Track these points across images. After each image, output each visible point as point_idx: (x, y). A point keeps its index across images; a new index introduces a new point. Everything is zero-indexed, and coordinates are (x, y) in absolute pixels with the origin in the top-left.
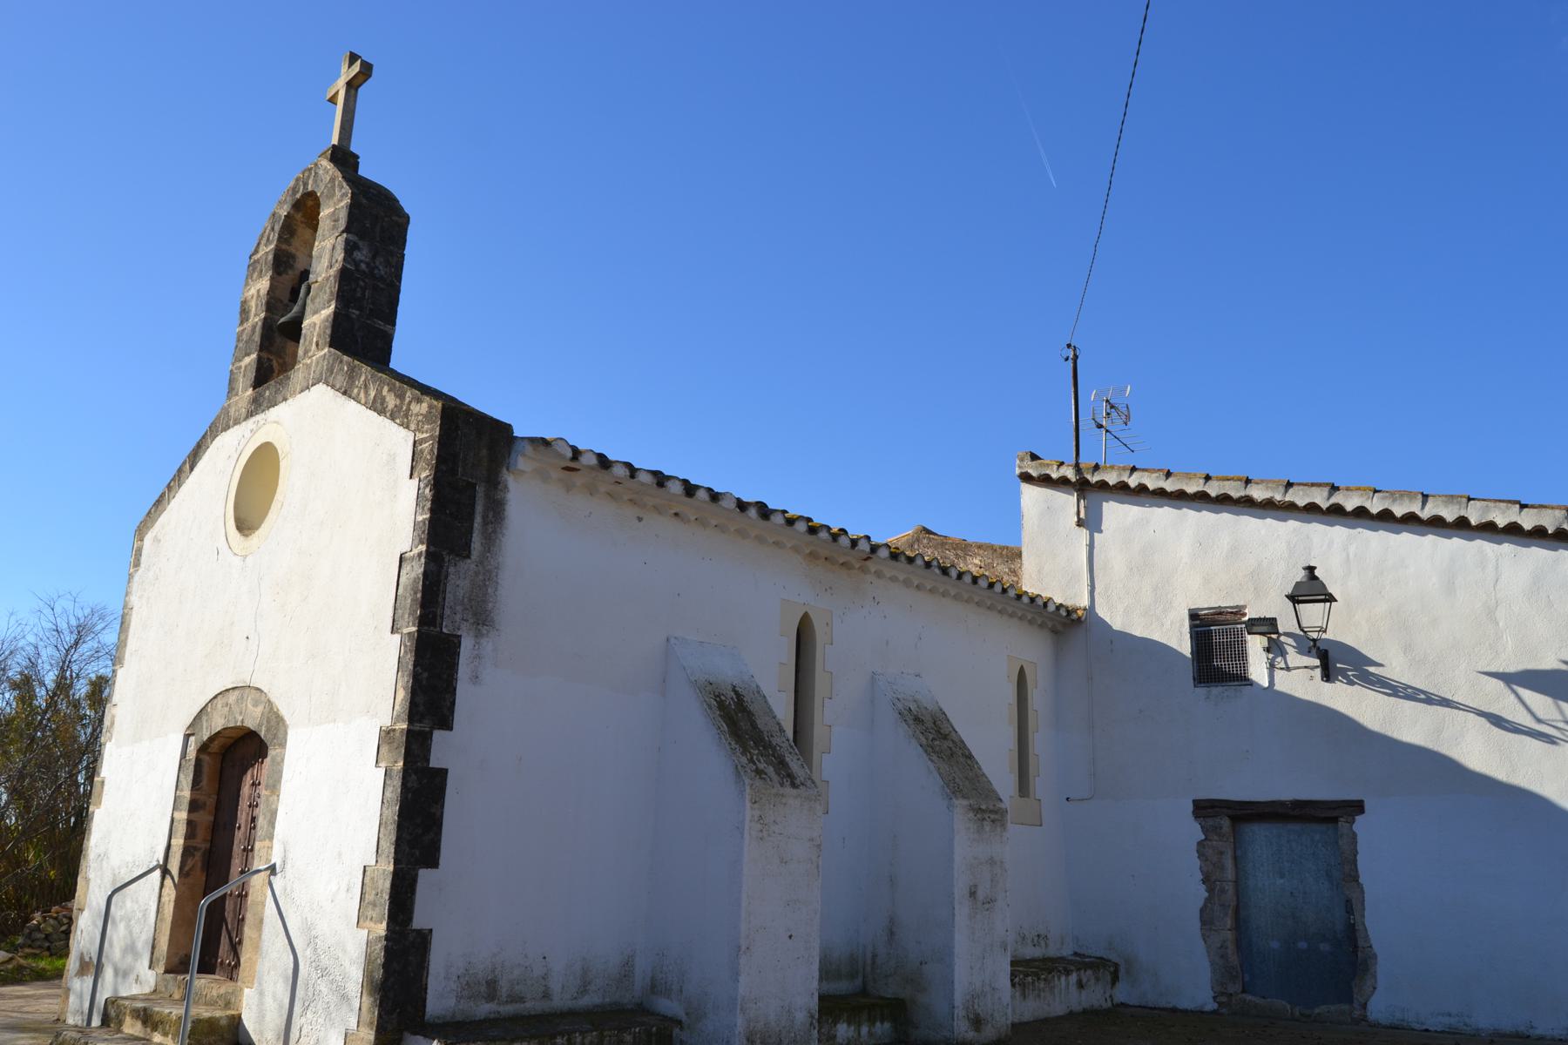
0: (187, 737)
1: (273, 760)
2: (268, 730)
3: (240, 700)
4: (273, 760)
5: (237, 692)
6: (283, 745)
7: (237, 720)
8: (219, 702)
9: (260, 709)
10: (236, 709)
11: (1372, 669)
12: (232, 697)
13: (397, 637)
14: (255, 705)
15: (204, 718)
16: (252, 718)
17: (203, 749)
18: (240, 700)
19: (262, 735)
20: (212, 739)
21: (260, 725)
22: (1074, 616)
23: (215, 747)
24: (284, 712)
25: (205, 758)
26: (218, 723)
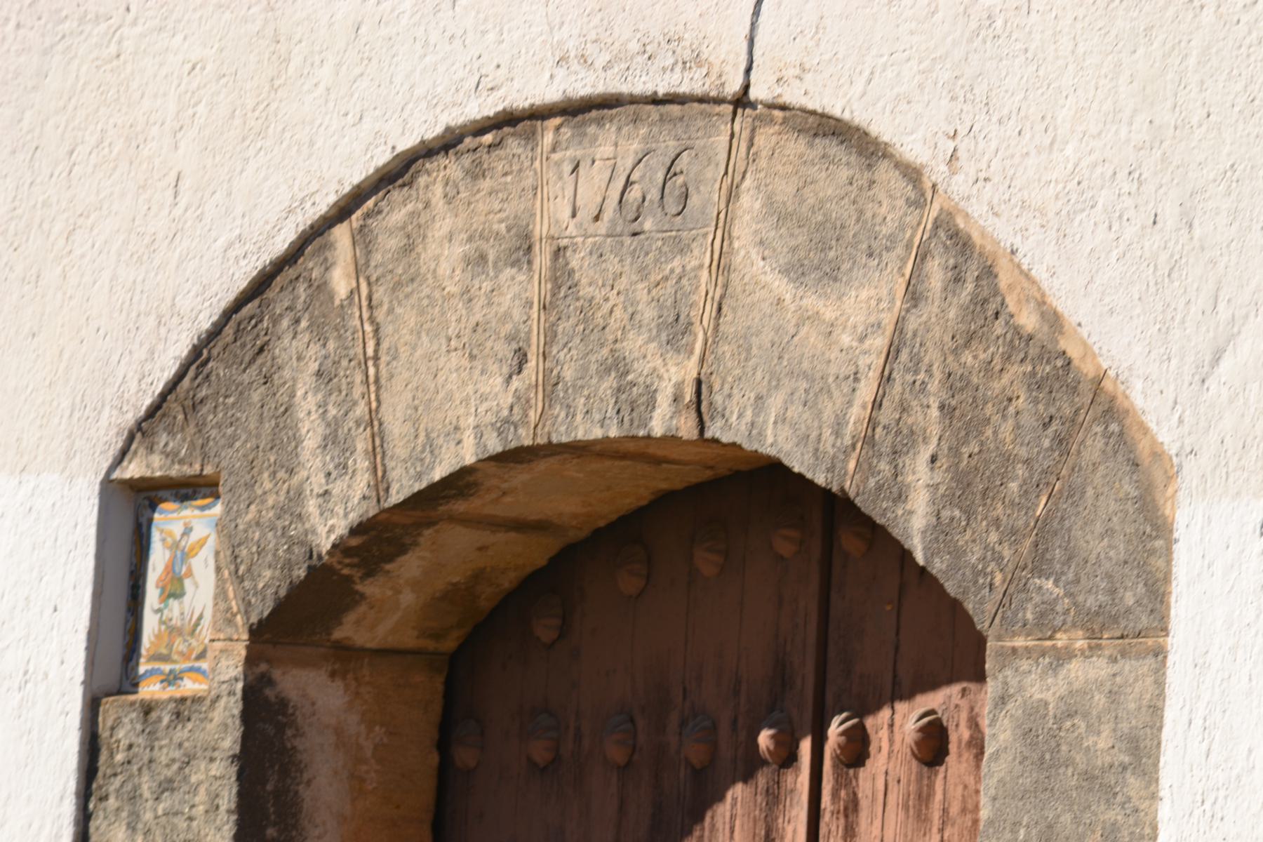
0: (130, 509)
1: (1044, 744)
2: (966, 489)
3: (654, 214)
4: (1044, 744)
5: (613, 145)
6: (1133, 618)
7: (644, 391)
8: (443, 219)
9: (862, 307)
10: (620, 293)
11: (844, 715)
12: (570, 190)
13: (876, 177)
14: (821, 257)
15: (298, 355)
16: (799, 374)
17: (299, 619)
18: (654, 214)
19: (914, 522)
20: (379, 538)
21: (883, 439)
22: (1149, 568)
23: (392, 608)
24: (1115, 337)
25: (317, 693)
26: (448, 400)
